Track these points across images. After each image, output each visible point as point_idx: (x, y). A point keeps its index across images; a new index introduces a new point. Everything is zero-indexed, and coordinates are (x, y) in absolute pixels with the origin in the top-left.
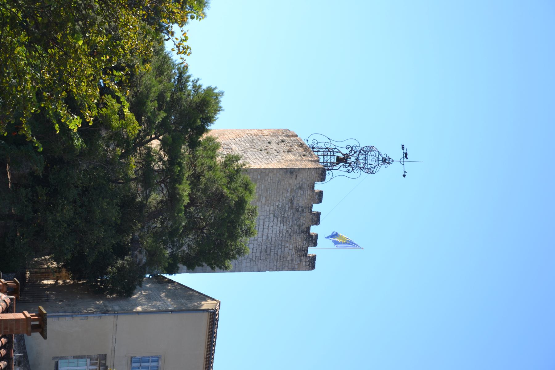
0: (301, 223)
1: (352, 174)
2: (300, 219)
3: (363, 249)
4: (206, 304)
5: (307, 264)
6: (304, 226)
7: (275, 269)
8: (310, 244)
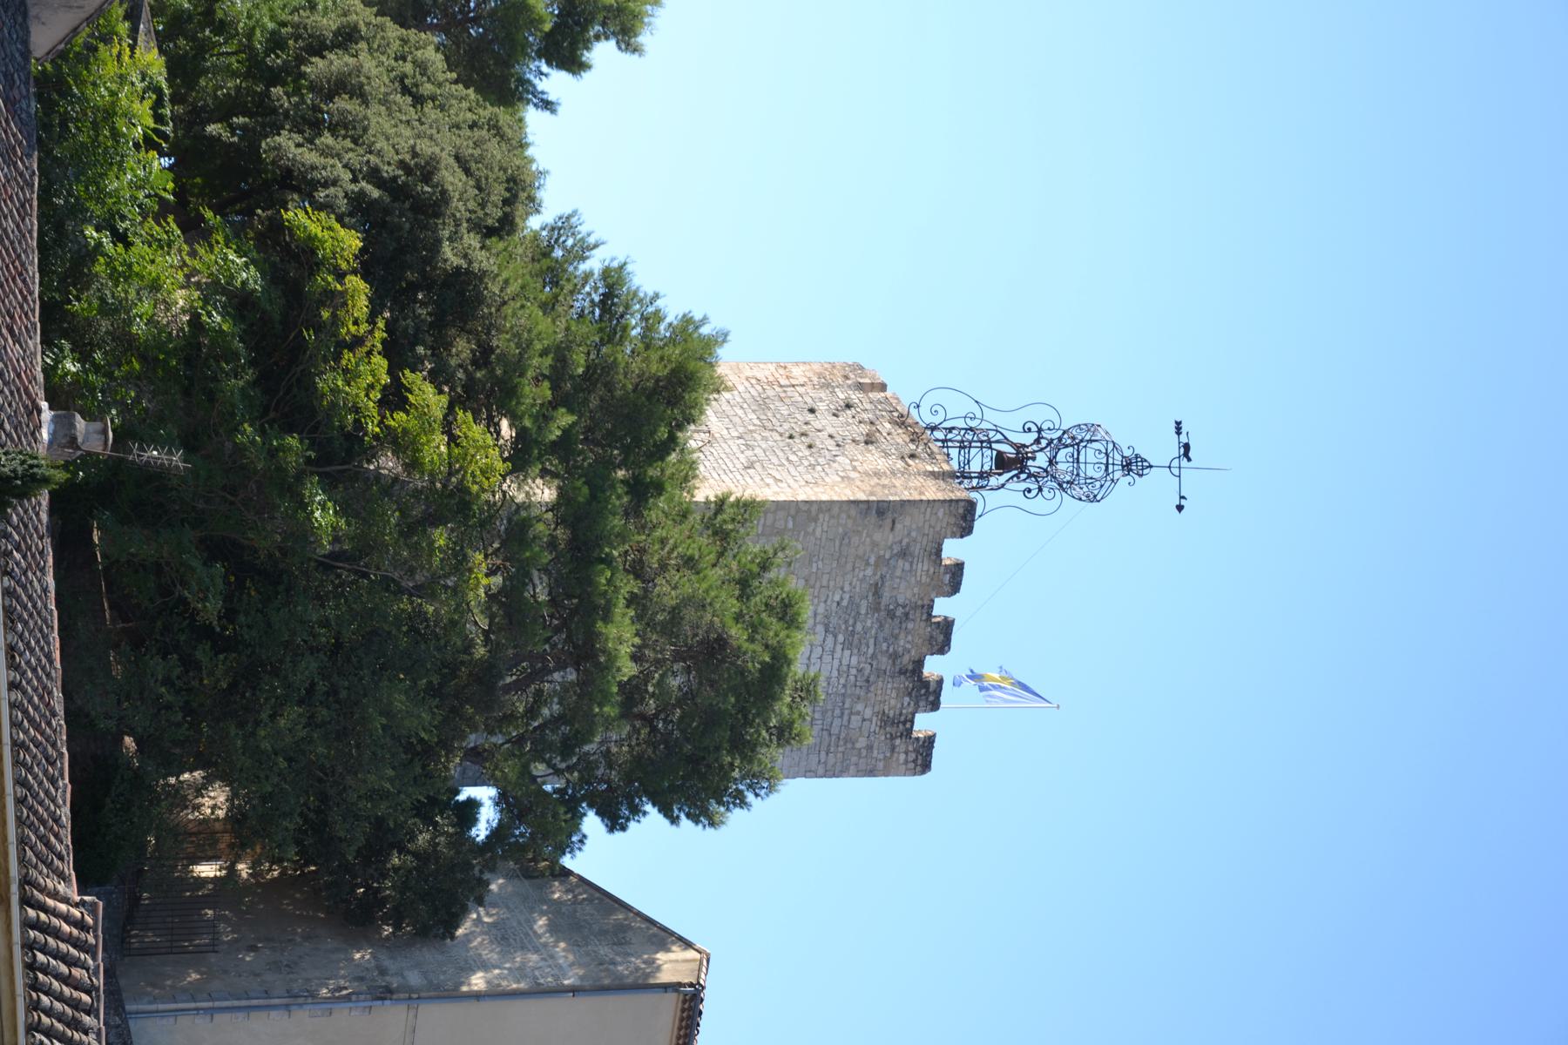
0: (900, 649)
1: (1038, 504)
2: (896, 637)
3: (1058, 707)
4: (671, 961)
5: (910, 759)
6: (906, 658)
7: (821, 771)
8: (922, 703)
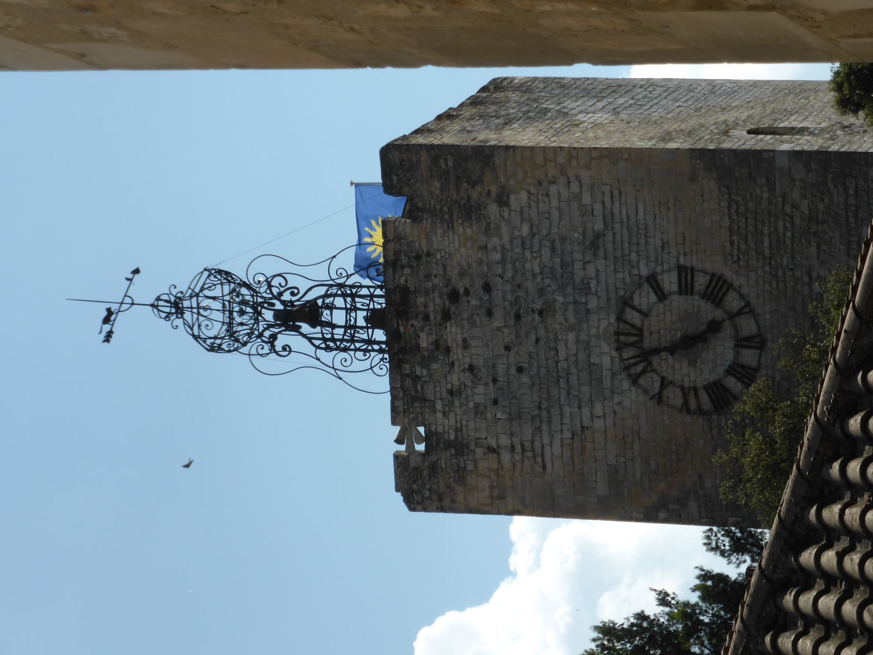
1: (270, 267)
